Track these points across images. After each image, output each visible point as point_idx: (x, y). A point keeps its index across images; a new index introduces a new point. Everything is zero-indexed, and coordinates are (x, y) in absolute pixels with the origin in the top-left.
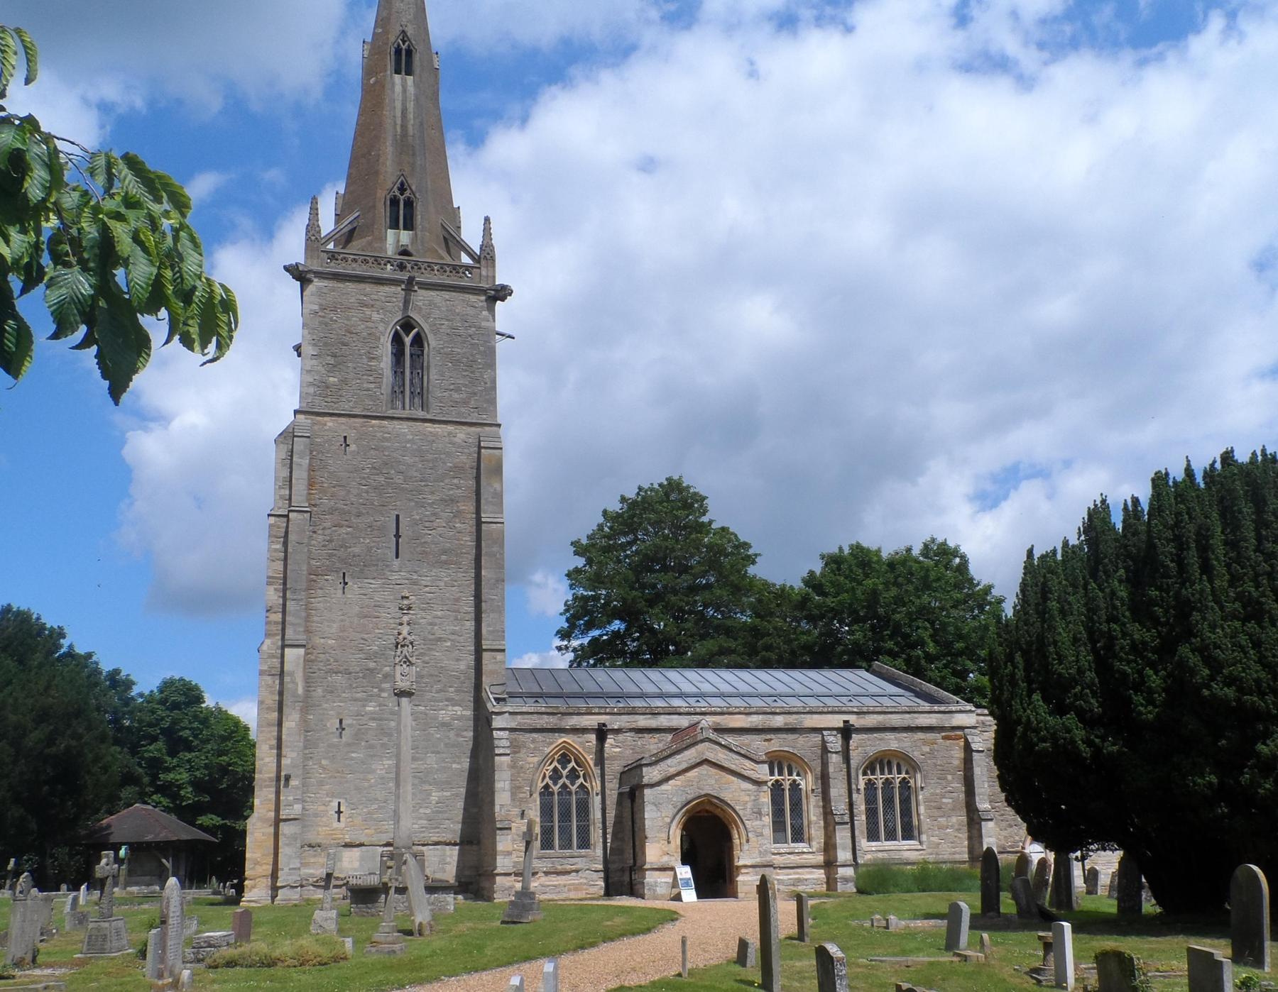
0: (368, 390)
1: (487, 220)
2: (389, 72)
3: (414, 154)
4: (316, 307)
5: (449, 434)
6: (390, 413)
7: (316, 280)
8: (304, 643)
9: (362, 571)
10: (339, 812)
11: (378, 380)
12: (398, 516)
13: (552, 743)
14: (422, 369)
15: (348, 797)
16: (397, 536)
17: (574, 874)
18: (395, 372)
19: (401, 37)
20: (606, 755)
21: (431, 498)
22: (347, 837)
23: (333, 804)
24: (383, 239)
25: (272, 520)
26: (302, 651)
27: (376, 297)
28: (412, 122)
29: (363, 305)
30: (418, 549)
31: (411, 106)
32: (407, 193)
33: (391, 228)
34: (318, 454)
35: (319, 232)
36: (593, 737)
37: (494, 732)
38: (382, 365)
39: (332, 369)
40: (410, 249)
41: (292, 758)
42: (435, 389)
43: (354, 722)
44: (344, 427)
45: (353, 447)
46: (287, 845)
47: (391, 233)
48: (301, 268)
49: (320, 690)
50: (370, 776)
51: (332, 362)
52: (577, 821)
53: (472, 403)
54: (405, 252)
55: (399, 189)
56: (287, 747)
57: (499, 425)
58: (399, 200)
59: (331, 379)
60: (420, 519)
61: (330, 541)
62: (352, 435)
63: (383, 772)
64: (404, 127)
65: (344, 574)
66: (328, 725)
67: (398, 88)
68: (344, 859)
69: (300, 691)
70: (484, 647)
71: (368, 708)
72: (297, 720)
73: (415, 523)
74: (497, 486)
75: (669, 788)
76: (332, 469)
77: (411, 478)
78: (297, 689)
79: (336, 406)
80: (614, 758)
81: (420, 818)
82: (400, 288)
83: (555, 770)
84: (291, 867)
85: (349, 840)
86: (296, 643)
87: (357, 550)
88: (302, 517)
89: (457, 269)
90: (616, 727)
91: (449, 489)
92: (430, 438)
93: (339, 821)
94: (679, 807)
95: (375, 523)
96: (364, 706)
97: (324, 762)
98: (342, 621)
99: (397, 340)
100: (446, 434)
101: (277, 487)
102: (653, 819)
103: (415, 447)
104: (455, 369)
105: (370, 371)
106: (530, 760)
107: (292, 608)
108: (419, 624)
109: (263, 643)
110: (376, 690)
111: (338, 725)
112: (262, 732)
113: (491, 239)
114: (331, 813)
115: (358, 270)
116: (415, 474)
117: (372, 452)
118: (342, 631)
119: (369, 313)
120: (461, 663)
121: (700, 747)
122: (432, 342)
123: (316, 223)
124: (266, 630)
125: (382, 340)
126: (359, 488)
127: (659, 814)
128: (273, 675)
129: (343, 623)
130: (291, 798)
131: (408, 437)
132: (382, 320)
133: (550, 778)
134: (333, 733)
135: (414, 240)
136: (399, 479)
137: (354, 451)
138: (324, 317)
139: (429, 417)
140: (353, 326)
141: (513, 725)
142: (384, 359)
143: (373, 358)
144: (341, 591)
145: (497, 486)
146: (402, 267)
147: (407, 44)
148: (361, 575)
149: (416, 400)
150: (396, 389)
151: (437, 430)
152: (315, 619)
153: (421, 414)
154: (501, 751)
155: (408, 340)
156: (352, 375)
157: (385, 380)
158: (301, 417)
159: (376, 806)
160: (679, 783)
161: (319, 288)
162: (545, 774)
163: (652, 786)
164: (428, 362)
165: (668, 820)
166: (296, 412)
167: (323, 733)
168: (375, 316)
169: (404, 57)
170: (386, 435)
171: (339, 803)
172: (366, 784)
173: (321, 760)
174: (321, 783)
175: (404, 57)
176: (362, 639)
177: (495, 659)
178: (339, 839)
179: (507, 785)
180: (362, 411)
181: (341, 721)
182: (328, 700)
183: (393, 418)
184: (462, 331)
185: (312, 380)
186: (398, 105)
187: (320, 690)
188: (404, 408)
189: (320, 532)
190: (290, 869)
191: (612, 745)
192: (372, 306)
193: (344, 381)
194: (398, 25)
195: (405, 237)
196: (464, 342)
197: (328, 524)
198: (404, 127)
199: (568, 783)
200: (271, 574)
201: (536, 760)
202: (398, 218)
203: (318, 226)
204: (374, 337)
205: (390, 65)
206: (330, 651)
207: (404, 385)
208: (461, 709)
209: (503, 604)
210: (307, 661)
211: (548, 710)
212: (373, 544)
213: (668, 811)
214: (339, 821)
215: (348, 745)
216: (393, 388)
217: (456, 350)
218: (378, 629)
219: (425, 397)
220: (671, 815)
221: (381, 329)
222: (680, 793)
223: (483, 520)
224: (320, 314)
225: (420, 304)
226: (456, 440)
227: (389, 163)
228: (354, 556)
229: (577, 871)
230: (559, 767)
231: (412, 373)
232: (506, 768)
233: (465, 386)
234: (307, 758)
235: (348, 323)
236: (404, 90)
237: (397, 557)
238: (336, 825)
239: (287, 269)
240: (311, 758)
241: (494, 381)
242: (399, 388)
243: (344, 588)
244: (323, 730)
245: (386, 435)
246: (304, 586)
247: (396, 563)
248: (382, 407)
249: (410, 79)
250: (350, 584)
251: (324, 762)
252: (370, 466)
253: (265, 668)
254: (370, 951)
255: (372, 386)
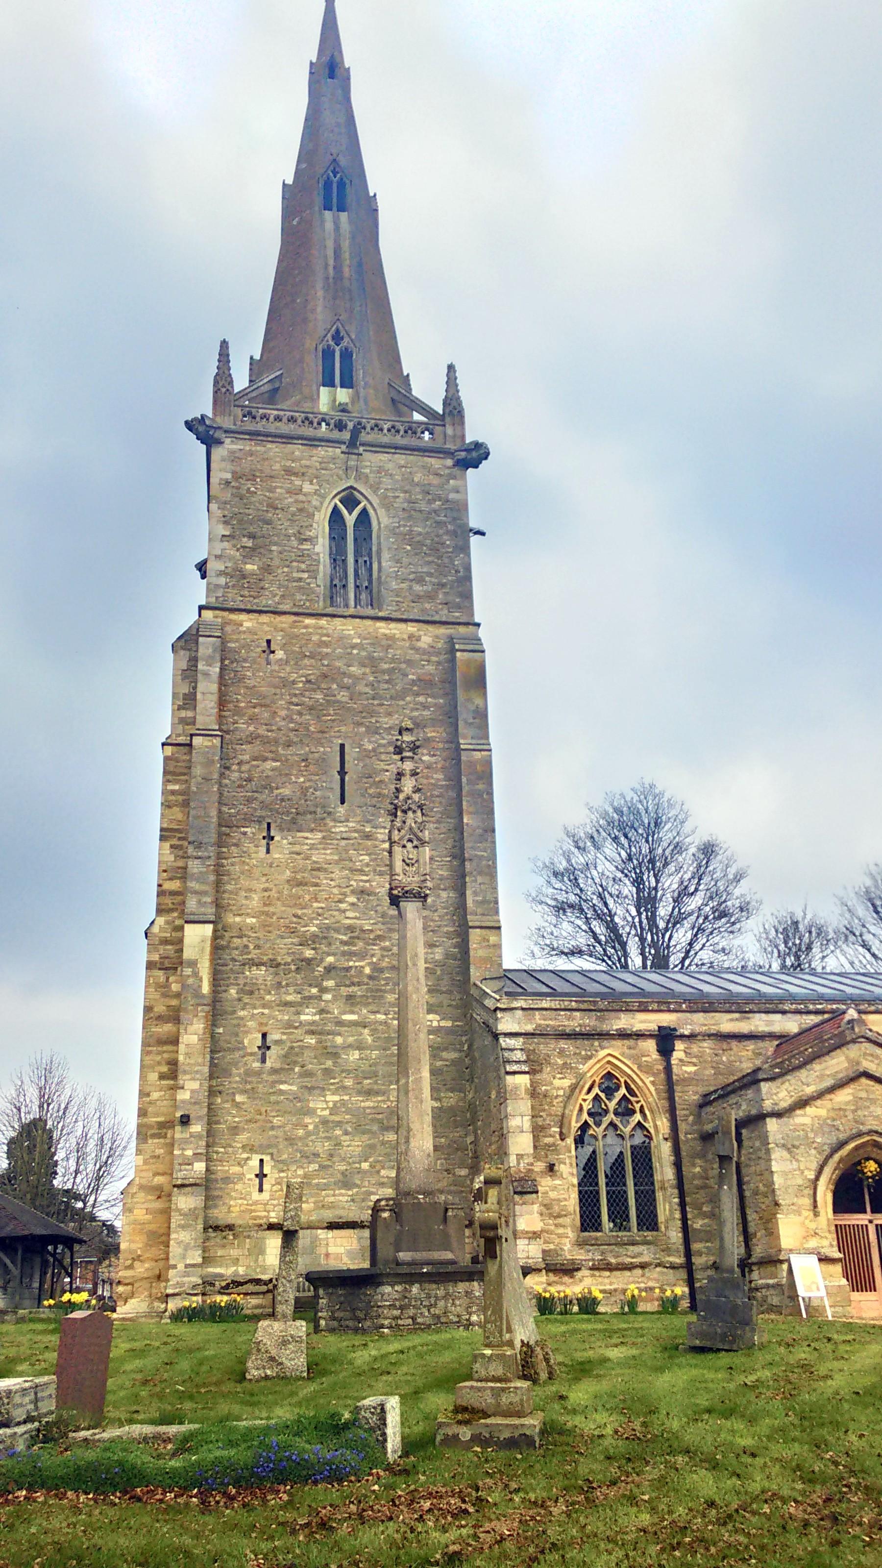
0: (300, 580)
1: (451, 368)
2: (317, 208)
3: (351, 299)
4: (229, 476)
5: (411, 637)
6: (330, 610)
7: (228, 441)
8: (212, 918)
9: (294, 821)
10: (261, 1176)
11: (312, 568)
12: (342, 746)
13: (590, 1057)
14: (370, 556)
15: (275, 1151)
16: (342, 772)
17: (639, 1271)
18: (335, 560)
19: (332, 168)
20: (674, 1077)
21: (386, 722)
22: (273, 1214)
23: (250, 1163)
24: (315, 398)
25: (169, 750)
26: (209, 928)
27: (308, 463)
28: (348, 262)
29: (289, 472)
30: (371, 791)
31: (346, 245)
32: (345, 343)
33: (324, 386)
34: (232, 662)
35: (231, 383)
36: (650, 1045)
37: (501, 1040)
38: (318, 549)
39: (250, 553)
40: (350, 407)
41: (192, 1091)
42: (388, 579)
43: (284, 1037)
44: (267, 629)
45: (280, 654)
46: (183, 1227)
47: (324, 391)
48: (208, 422)
49: (233, 991)
50: (307, 1120)
51: (250, 545)
52: (635, 1185)
53: (440, 596)
54: (344, 410)
55: (333, 338)
56: (185, 1072)
57: (478, 625)
58: (334, 351)
59: (249, 567)
60: (374, 750)
61: (249, 780)
62: (278, 639)
63: (327, 1112)
64: (338, 268)
65: (269, 825)
66: (246, 1042)
67: (329, 225)
68: (268, 1251)
69: (206, 989)
70: (470, 924)
71: (303, 1018)
72: (201, 1032)
73: (366, 755)
74: (478, 701)
75: (807, 1120)
76: (250, 683)
77: (360, 694)
78: (200, 987)
79: (255, 601)
80: (688, 1081)
81: (382, 1185)
82: (338, 451)
83: (597, 1098)
84: (188, 1262)
85: (275, 1220)
86: (202, 918)
87: (286, 791)
88: (210, 744)
89: (412, 429)
90: (687, 1033)
91: (412, 710)
92: (384, 642)
93: (261, 1190)
94: (826, 1153)
95: (311, 756)
96: (298, 1013)
97: (239, 1098)
98: (265, 890)
99: (336, 517)
100: (406, 637)
101: (176, 707)
102: (785, 1174)
103: (364, 654)
104: (416, 554)
105: (302, 556)
106: (557, 1083)
107: (195, 870)
108: (376, 894)
109: (153, 922)
110: (314, 991)
111: (259, 1043)
112: (149, 1053)
113: (458, 391)
114: (248, 1176)
115: (284, 428)
116: (367, 690)
117: (306, 661)
118: (265, 905)
119: (300, 483)
120: (437, 950)
121: (853, 1051)
122: (381, 519)
123: (226, 372)
124: (158, 904)
125: (316, 517)
126: (288, 709)
127: (795, 1165)
128: (166, 969)
129: (266, 894)
130: (189, 1153)
131: (354, 641)
132: (316, 492)
133: (590, 1114)
134: (252, 1054)
135: (355, 398)
136: (343, 696)
137: (281, 659)
138: (238, 488)
139: (381, 614)
140: (277, 499)
141: (529, 1028)
142: (320, 540)
143: (305, 540)
144: (264, 850)
145: (478, 701)
146: (340, 426)
147: (338, 176)
148: (293, 825)
149: (363, 596)
150: (336, 582)
151: (393, 631)
152: (229, 887)
153: (370, 612)
154: (515, 1068)
155: (350, 519)
156: (276, 562)
157: (321, 567)
158: (208, 615)
159: (316, 1166)
160: (823, 1112)
161: (232, 452)
162: (581, 1106)
163: (778, 1115)
164: (379, 544)
165: (811, 1175)
166: (201, 608)
167: (237, 1054)
168: (307, 488)
169: (335, 200)
170: (324, 639)
171: (261, 1161)
172: (301, 1132)
173: (234, 1094)
174: (235, 1130)
175: (335, 200)
176: (295, 916)
177: (488, 941)
178: (260, 1218)
179: (527, 1123)
180: (292, 608)
181: (264, 1036)
182: (246, 1004)
183: (334, 616)
184: (423, 506)
185: (223, 568)
186: (330, 244)
187: (233, 991)
188: (347, 606)
189: (235, 767)
190: (187, 1266)
191: (681, 1060)
192: (303, 474)
193: (267, 569)
194: (328, 154)
195: (343, 395)
196: (427, 519)
197: (246, 757)
198: (338, 268)
199: (617, 1121)
200: (165, 826)
201: (566, 1083)
202: (333, 370)
203: (230, 375)
204: (306, 513)
205: (318, 200)
206: (250, 933)
207: (346, 577)
208: (438, 1017)
209: (495, 863)
210: (218, 947)
211: (582, 1006)
212: (308, 784)
213: (809, 1162)
214: (261, 1190)
215: (274, 1071)
216: (332, 581)
217: (416, 529)
218: (317, 901)
219: (375, 590)
220: (814, 1166)
221: (315, 503)
222: (826, 1129)
223: (462, 747)
224: (233, 484)
225: (367, 471)
226: (420, 644)
227: (319, 309)
228: (282, 800)
229: (643, 1266)
230: (603, 1095)
231: (356, 561)
232: (523, 1095)
233: (430, 575)
234: (212, 1093)
235: (271, 495)
236: (337, 227)
237: (343, 802)
238: (256, 1196)
239: (189, 425)
240: (220, 1093)
241: (468, 568)
242: (340, 580)
243: (268, 844)
244: (239, 1049)
245: (324, 639)
246: (213, 837)
247: (341, 810)
248: (318, 602)
249: (344, 216)
250: (276, 838)
251: (239, 1098)
252: (304, 679)
253: (156, 957)
254: (456, 1437)
255: (306, 575)
